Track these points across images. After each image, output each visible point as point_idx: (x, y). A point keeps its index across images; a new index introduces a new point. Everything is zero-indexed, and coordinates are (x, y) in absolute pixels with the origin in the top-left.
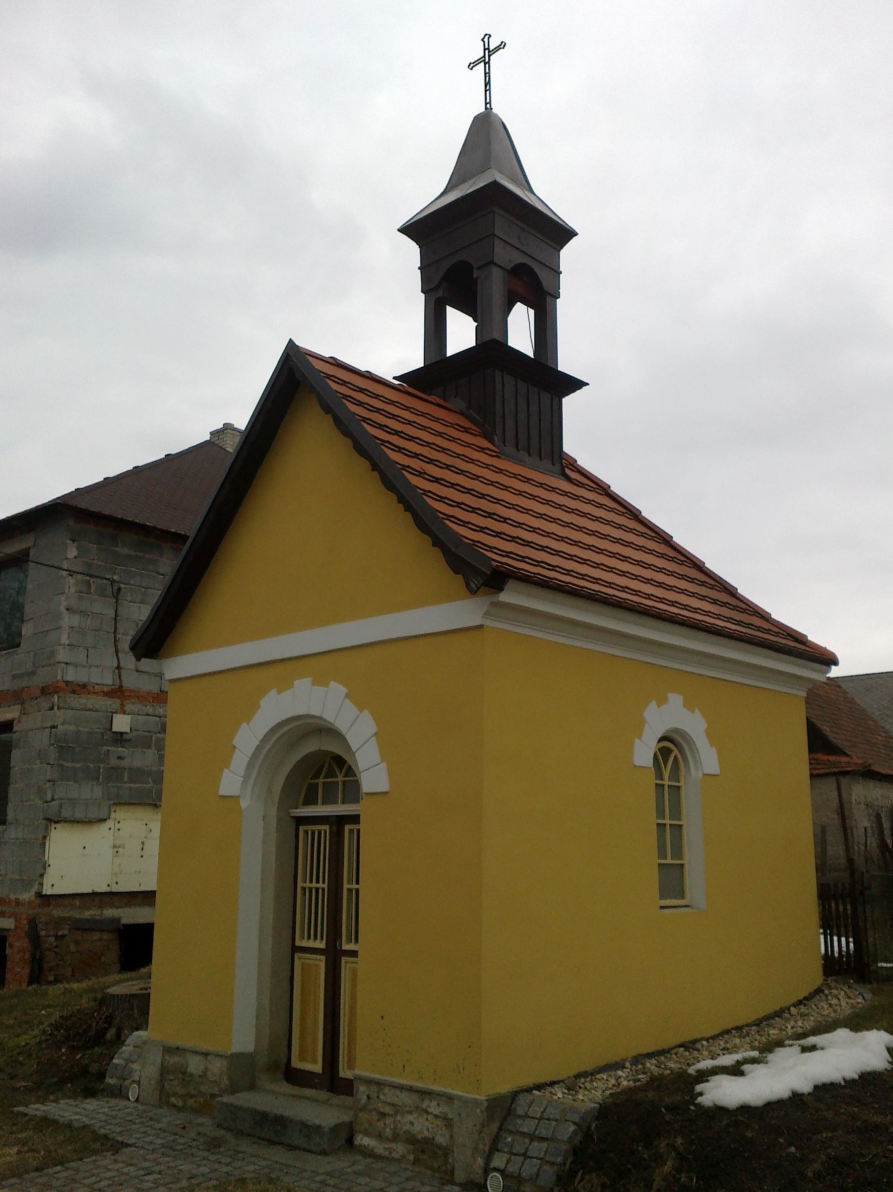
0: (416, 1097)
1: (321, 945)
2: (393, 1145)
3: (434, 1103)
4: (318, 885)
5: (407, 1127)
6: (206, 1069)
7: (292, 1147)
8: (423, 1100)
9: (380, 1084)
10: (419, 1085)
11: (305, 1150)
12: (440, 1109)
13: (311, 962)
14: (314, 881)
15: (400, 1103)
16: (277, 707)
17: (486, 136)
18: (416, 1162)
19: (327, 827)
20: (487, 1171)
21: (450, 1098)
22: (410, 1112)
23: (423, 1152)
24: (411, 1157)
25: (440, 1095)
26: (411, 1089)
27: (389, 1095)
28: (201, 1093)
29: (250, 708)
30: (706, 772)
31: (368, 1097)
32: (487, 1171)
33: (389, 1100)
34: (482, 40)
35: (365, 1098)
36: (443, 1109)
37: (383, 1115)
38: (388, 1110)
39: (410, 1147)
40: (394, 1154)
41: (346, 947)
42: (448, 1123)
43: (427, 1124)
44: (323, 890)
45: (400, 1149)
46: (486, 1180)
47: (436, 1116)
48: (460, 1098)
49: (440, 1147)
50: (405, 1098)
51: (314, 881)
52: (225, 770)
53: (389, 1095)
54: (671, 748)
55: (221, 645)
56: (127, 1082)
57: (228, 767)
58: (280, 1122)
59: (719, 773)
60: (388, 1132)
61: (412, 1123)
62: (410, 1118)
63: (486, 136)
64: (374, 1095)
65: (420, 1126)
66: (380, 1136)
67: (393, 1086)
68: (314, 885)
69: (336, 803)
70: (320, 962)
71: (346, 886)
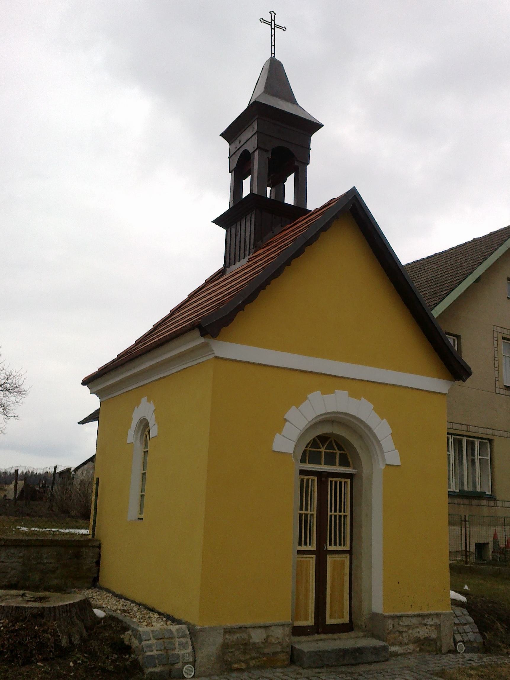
0: (420, 619)
1: (314, 548)
2: (408, 646)
3: (430, 619)
4: (340, 514)
5: (417, 634)
6: (268, 636)
7: (370, 663)
8: (424, 619)
9: (400, 617)
10: (421, 612)
11: (375, 662)
12: (434, 622)
13: (304, 559)
14: (333, 511)
15: (412, 624)
16: (340, 402)
17: (275, 76)
18: (421, 650)
19: (316, 478)
20: (455, 643)
21: (438, 615)
22: (417, 627)
23: (423, 645)
24: (418, 649)
25: (433, 615)
26: (419, 616)
27: (406, 622)
28: (264, 654)
29: (299, 398)
30: (388, 463)
31: (393, 626)
32: (455, 643)
33: (406, 624)
34: (275, 14)
35: (392, 626)
36: (436, 620)
37: (401, 633)
38: (405, 629)
39: (416, 644)
40: (409, 651)
41: (330, 548)
42: (438, 627)
43: (428, 630)
44: (312, 515)
45: (411, 647)
46: (456, 647)
47: (431, 625)
48: (443, 614)
49: (432, 640)
50: (415, 621)
51: (333, 511)
52: (277, 435)
53: (406, 622)
54: (333, 448)
55: (257, 345)
56: (179, 665)
57: (280, 433)
58: (359, 650)
59: (400, 464)
60: (406, 640)
61: (419, 632)
62: (418, 630)
63: (275, 76)
64: (396, 624)
65: (422, 632)
66: (401, 644)
67: (408, 616)
68: (338, 513)
69: (320, 464)
70: (312, 560)
71: (315, 512)
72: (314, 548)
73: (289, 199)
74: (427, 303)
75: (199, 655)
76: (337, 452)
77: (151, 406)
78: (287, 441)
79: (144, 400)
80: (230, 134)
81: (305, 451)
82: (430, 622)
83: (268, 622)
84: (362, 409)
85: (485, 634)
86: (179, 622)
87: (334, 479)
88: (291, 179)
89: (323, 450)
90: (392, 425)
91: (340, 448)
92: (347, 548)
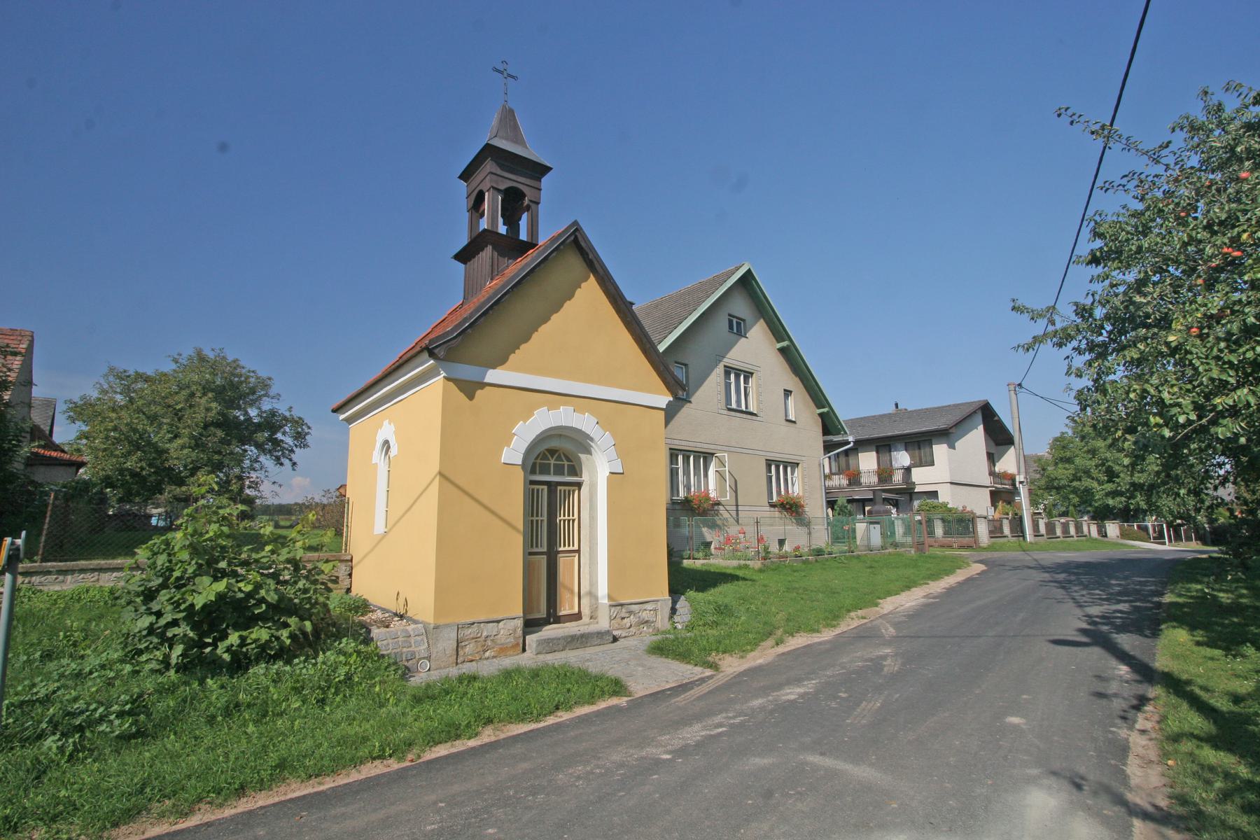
1: (545, 550)
19: (545, 488)
29: (527, 414)
41: (562, 549)
71: (545, 518)
72: (545, 550)
73: (523, 236)
74: (654, 338)
75: (434, 651)
76: (566, 463)
77: (392, 427)
78: (514, 453)
79: (386, 423)
80: (466, 175)
81: (534, 464)
82: (649, 606)
83: (500, 618)
84: (584, 422)
85: (1121, 607)
86: (416, 622)
87: (562, 488)
88: (525, 217)
89: (552, 462)
90: (614, 435)
91: (569, 460)
92: (576, 547)
